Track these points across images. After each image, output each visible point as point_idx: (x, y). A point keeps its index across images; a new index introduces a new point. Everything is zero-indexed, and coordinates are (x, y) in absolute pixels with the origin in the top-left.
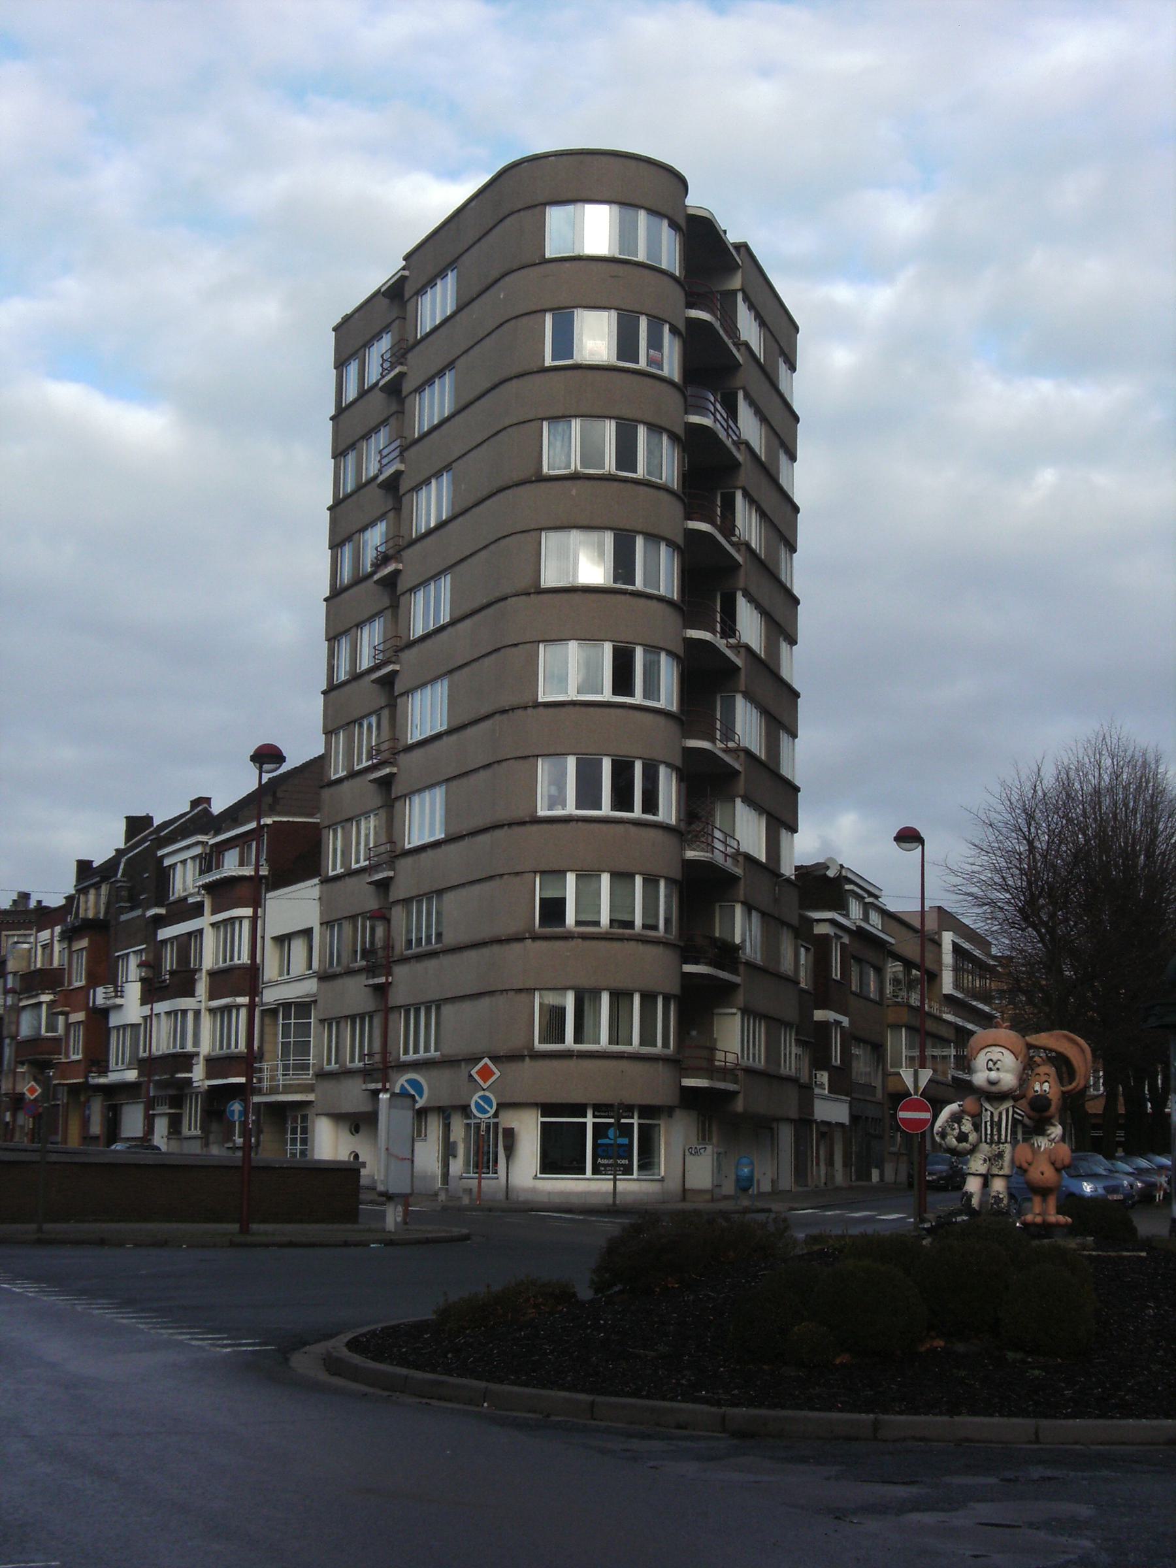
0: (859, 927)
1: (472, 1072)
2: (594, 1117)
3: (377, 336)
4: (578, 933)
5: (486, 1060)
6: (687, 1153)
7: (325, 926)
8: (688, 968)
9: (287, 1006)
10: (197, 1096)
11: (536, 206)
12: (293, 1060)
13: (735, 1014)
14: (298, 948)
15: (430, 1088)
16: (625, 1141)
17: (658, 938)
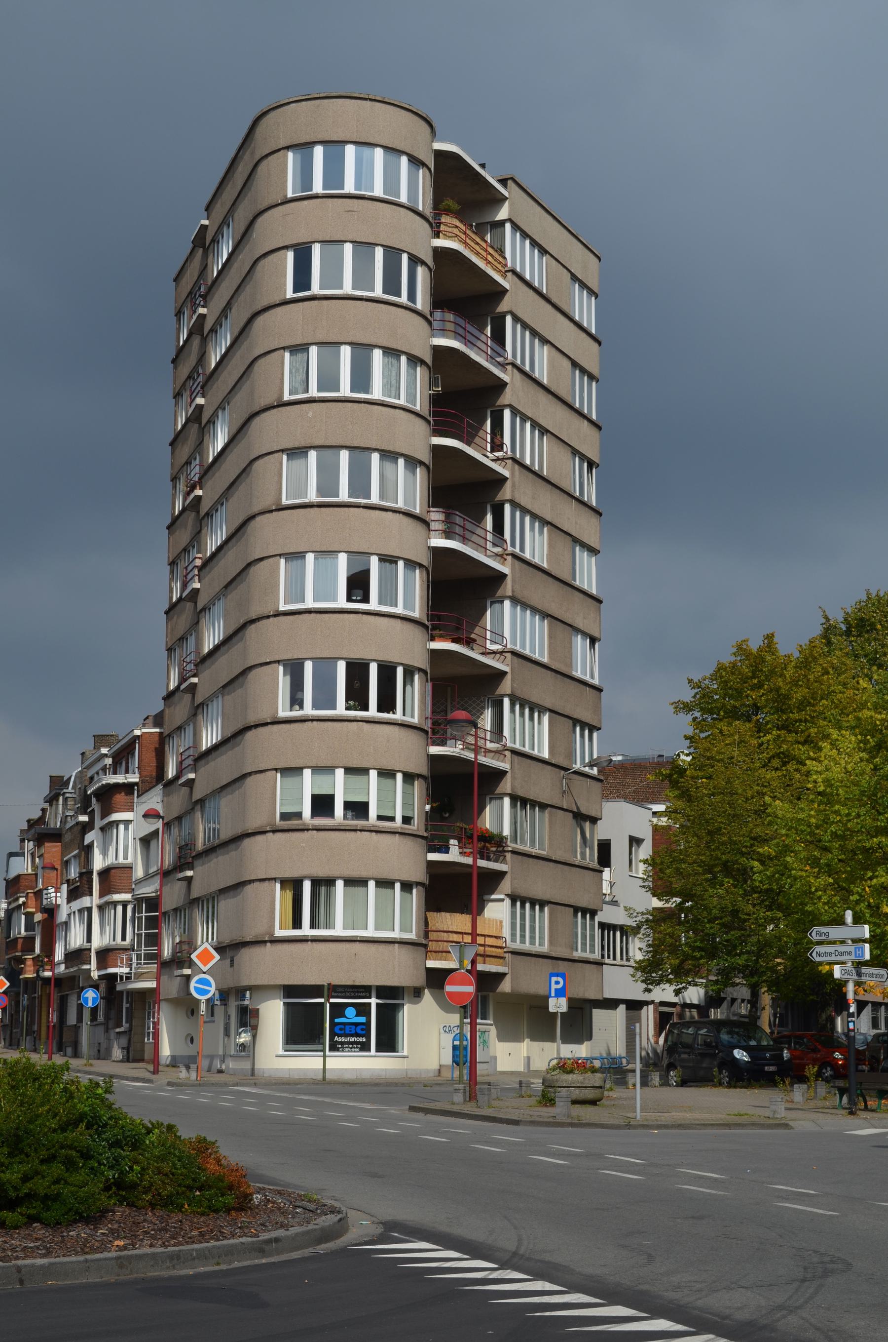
4: (313, 825)
13: (502, 900)
15: (212, 976)
16: (362, 1020)
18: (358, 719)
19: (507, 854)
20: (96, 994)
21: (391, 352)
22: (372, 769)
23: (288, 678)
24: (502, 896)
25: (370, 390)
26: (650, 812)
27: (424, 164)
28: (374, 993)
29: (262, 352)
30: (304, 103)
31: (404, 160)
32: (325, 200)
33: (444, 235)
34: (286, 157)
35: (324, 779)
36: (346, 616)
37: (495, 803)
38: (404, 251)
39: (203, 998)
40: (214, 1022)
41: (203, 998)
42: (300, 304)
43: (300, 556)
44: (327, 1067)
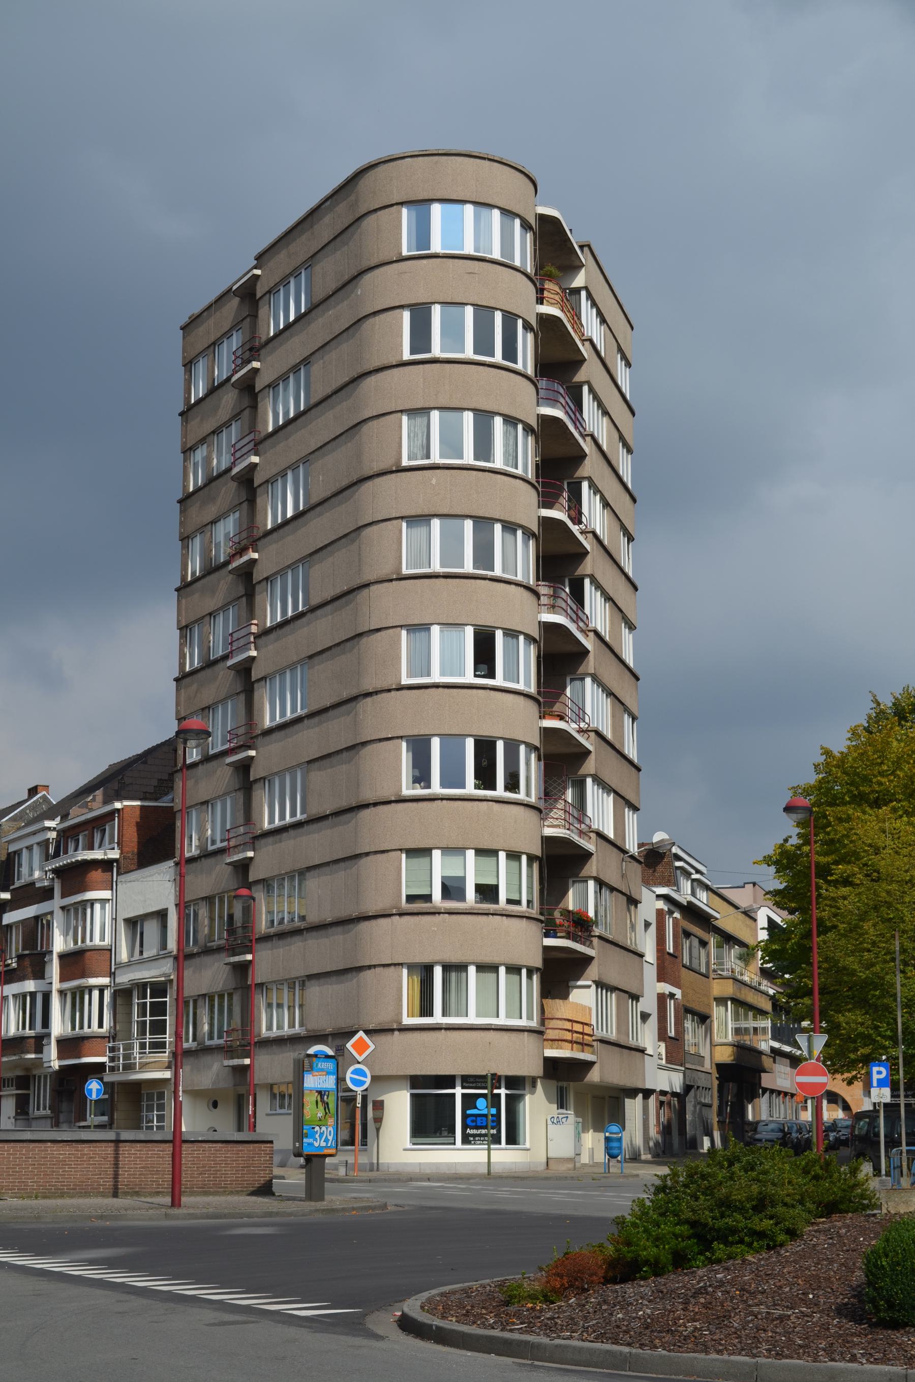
0: (689, 903)
2: (463, 1088)
3: (227, 334)
4: (445, 909)
5: (361, 1034)
6: (549, 1122)
8: (549, 942)
9: (142, 987)
10: (45, 1077)
11: (392, 205)
12: (150, 1039)
13: (589, 987)
14: (151, 929)
17: (523, 912)
18: (489, 798)
19: (593, 939)
20: (101, 1086)
21: (511, 421)
22: (501, 850)
23: (410, 754)
24: (589, 983)
25: (492, 459)
26: (654, 896)
27: (531, 228)
28: (458, 1082)
29: (375, 414)
30: (421, 159)
31: (517, 222)
32: (445, 260)
33: (547, 301)
34: (400, 213)
35: (456, 860)
36: (474, 691)
37: (578, 886)
38: (520, 317)
39: (359, 1090)
41: (359, 1090)
42: (421, 366)
43: (425, 628)
44: (492, 1161)
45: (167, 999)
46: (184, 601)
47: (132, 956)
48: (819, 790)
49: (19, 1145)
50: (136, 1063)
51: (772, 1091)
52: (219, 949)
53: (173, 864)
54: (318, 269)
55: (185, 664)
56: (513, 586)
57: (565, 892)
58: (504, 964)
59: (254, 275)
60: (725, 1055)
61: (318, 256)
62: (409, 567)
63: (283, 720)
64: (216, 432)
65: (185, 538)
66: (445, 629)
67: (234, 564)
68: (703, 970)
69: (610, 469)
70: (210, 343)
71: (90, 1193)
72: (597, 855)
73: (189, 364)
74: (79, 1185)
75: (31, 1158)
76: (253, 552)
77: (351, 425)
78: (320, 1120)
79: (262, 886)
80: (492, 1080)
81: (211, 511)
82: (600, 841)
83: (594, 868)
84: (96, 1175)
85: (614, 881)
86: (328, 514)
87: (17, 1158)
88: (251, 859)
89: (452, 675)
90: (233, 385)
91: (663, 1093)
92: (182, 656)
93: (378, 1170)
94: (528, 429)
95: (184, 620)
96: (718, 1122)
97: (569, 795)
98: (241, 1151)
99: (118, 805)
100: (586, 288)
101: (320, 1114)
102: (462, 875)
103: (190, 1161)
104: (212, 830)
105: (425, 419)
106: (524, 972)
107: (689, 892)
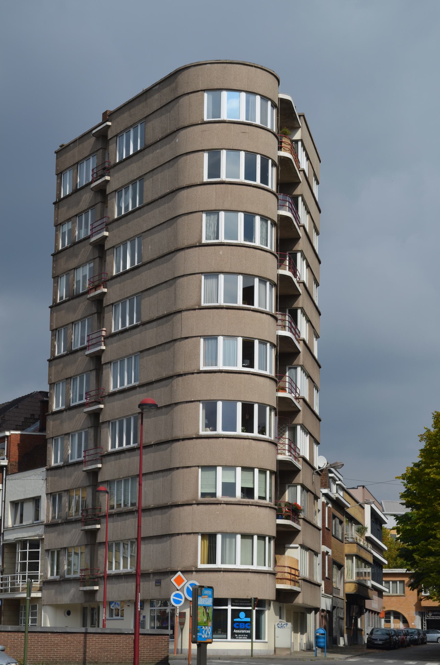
1: (171, 580)
2: (232, 606)
5: (179, 573)
6: (276, 627)
7: (49, 495)
8: (280, 521)
9: (23, 543)
11: (198, 91)
12: (28, 573)
13: (297, 548)
14: (29, 509)
16: (248, 620)
19: (300, 520)
21: (264, 219)
22: (256, 468)
23: (204, 411)
24: (297, 545)
25: (254, 240)
28: (229, 602)
30: (216, 65)
31: (269, 103)
33: (284, 149)
34: (203, 96)
35: (230, 473)
36: (242, 375)
38: (270, 158)
40: (123, 619)
42: (214, 185)
43: (214, 337)
44: (254, 648)
45: (40, 550)
46: (55, 314)
47: (15, 524)
48: (436, 437)
49: (34, 634)
50: (19, 588)
51: (370, 611)
52: (76, 521)
53: (45, 470)
54: (150, 125)
55: (55, 351)
56: (265, 315)
57: (284, 492)
58: (257, 534)
59: (107, 125)
60: (351, 589)
61: (150, 117)
62: (205, 302)
63: (122, 388)
64: (78, 215)
65: (56, 277)
66: (227, 338)
67: (92, 295)
68: (340, 538)
69: (310, 245)
70: (75, 162)
71: (71, 662)
72: (303, 471)
73: (60, 174)
74: (65, 658)
75: (40, 642)
76: (103, 288)
77: (171, 218)
78: (205, 623)
79: (107, 485)
80: (254, 601)
81: (74, 263)
82: (304, 463)
83: (301, 478)
84: (74, 652)
85: (309, 487)
86: (155, 269)
87: (33, 642)
88: (100, 468)
89: (229, 365)
90: (91, 189)
91: (323, 611)
92: (53, 347)
93: (181, 653)
94: (274, 224)
95: (55, 325)
96: (346, 628)
97: (287, 435)
98: (152, 639)
99: (7, 433)
100: (301, 140)
101: (205, 620)
102: (234, 482)
103: (125, 645)
104: (71, 450)
105: (216, 216)
106: (267, 539)
107: (335, 492)
